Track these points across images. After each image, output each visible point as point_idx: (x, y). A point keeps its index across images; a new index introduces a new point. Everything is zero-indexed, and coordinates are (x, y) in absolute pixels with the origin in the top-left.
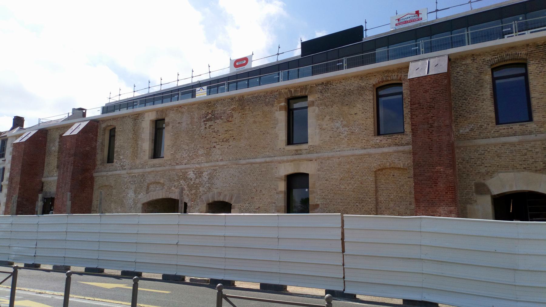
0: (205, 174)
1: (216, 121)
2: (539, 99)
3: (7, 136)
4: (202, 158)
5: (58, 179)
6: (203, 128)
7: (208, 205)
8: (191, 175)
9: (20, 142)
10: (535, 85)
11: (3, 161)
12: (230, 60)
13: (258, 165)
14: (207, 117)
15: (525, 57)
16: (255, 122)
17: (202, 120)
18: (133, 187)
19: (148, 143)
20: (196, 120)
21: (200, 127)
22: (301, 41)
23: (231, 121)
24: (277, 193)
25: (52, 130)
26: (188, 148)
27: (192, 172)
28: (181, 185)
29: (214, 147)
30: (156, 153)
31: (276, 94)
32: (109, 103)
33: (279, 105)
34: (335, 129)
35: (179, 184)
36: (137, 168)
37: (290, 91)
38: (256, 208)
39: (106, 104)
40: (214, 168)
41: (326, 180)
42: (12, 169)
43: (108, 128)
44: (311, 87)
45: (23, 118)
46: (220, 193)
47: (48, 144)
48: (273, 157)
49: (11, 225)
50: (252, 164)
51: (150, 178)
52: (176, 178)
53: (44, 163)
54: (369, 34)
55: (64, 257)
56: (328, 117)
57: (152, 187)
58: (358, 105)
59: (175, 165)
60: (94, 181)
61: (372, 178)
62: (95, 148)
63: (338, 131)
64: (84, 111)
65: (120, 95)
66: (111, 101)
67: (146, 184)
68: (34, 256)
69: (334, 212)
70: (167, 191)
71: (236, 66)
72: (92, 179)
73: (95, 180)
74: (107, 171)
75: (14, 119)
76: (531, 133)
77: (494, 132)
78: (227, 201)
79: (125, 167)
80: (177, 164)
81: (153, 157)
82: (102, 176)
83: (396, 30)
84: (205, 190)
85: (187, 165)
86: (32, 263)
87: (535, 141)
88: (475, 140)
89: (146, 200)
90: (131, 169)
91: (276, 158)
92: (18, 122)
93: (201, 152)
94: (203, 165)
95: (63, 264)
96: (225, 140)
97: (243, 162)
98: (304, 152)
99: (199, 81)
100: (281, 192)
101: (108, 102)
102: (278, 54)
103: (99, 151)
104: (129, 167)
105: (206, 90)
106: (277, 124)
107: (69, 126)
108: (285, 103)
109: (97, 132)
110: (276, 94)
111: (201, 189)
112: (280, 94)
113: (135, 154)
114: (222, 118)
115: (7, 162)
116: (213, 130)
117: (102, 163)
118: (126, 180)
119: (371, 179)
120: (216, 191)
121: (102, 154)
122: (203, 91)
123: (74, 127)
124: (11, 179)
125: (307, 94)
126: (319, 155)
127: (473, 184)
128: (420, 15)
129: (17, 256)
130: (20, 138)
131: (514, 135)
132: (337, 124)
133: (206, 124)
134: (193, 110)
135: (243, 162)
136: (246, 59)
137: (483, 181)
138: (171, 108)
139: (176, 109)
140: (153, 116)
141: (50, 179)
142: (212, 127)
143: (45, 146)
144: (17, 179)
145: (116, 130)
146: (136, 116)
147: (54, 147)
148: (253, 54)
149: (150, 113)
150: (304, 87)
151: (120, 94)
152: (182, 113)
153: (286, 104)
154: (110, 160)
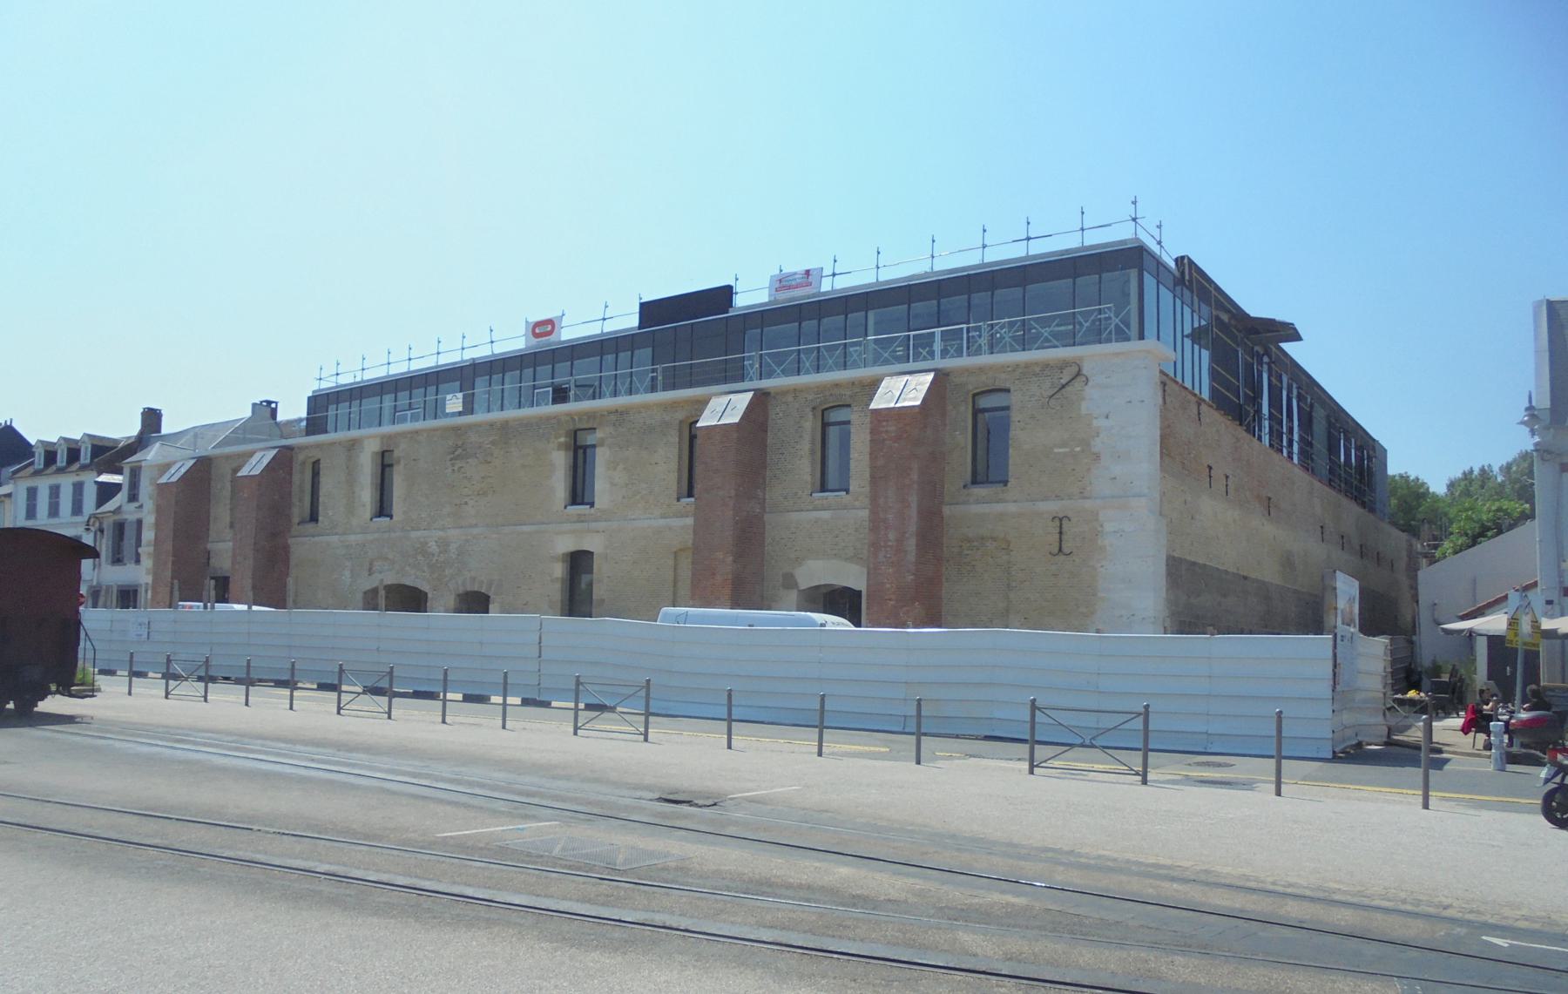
6: (450, 470)
9: (170, 481)
14: (456, 453)
19: (369, 490)
22: (641, 299)
27: (434, 543)
29: (466, 503)
30: (383, 509)
31: (553, 421)
33: (556, 442)
39: (314, 392)
42: (157, 525)
45: (160, 410)
46: (473, 579)
54: (741, 301)
56: (621, 467)
61: (671, 562)
64: (273, 405)
66: (325, 385)
71: (536, 335)
73: (292, 550)
80: (413, 529)
83: (775, 301)
99: (473, 359)
100: (557, 578)
101: (316, 388)
103: (295, 500)
105: (461, 400)
108: (566, 437)
109: (291, 469)
110: (553, 421)
111: (447, 572)
115: (145, 509)
121: (300, 508)
123: (254, 460)
124: (157, 542)
136: (550, 322)
138: (403, 435)
140: (371, 448)
141: (221, 546)
142: (463, 470)
147: (222, 489)
150: (591, 415)
153: (568, 439)
154: (314, 518)
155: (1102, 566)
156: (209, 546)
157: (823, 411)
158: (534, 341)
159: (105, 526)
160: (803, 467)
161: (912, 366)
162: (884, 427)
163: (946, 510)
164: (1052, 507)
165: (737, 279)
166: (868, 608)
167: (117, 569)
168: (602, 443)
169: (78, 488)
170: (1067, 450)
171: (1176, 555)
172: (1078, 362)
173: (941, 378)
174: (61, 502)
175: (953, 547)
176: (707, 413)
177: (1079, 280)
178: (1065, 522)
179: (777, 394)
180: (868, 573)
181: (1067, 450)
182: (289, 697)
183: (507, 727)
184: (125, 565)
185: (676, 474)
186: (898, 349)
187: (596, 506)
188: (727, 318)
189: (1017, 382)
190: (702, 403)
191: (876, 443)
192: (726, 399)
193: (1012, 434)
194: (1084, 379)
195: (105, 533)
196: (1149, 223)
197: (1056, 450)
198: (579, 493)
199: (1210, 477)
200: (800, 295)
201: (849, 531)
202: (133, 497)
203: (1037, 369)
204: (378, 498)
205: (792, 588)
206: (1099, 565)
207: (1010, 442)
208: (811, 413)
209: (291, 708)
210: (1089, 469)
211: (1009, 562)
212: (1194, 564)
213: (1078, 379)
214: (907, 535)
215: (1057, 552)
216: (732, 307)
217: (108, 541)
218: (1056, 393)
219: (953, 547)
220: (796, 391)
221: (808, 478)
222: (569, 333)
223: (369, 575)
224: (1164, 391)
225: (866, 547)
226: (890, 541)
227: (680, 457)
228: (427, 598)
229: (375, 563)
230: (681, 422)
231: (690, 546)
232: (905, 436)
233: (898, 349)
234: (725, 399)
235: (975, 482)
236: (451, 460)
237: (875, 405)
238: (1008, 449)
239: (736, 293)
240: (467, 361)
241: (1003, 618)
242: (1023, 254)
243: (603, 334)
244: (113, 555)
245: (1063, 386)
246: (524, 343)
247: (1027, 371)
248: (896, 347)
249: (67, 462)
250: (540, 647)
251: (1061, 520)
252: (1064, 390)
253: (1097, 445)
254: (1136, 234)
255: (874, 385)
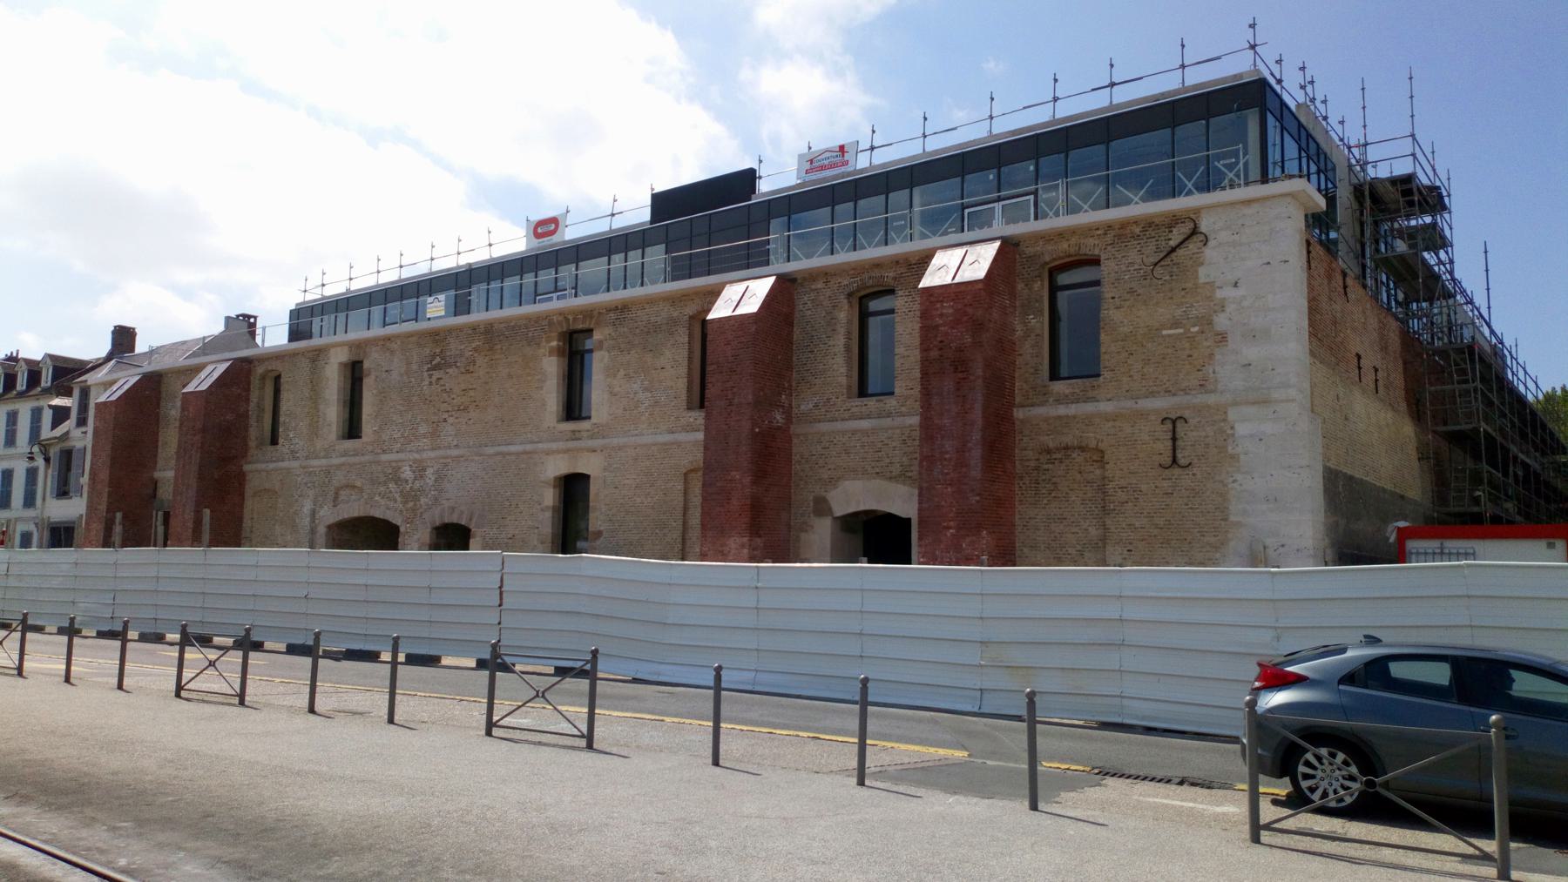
0: (429, 471)
1: (448, 370)
2: (904, 357)
3: (89, 383)
4: (425, 440)
5: (176, 478)
7: (434, 531)
8: (407, 473)
10: (901, 332)
11: (82, 433)
12: (525, 222)
13: (513, 458)
14: (434, 363)
15: (892, 282)
16: (510, 376)
17: (426, 368)
18: (311, 493)
20: (415, 367)
21: (422, 380)
22: (653, 190)
23: (472, 372)
24: (542, 510)
25: (170, 375)
26: (401, 421)
27: (408, 468)
28: (391, 492)
29: (445, 420)
30: (352, 429)
32: (304, 303)
34: (631, 396)
35: (388, 491)
36: (317, 457)
37: (567, 320)
38: (509, 536)
39: (297, 305)
40: (445, 461)
41: (616, 488)
43: (270, 374)
44: (600, 313)
45: (134, 329)
46: (453, 509)
47: (163, 404)
48: (536, 443)
49: (74, 565)
50: (503, 454)
51: (339, 478)
52: (382, 479)
53: (157, 441)
54: (766, 186)
55: (156, 619)
57: (343, 494)
58: (667, 352)
59: (379, 454)
60: (244, 480)
61: (680, 487)
62: (246, 415)
63: (636, 399)
64: (252, 320)
65: (323, 285)
66: (310, 297)
67: (332, 488)
68: (112, 618)
69: (1186, 563)
70: (366, 503)
71: (537, 235)
72: (241, 478)
73: (247, 478)
74: (267, 462)
75: (113, 333)
76: (889, 415)
77: (845, 410)
78: (463, 523)
79: (298, 455)
80: (384, 452)
81: (347, 435)
82: (259, 472)
84: (430, 503)
85: (400, 454)
86: (107, 630)
87: (892, 428)
88: (817, 425)
89: (332, 520)
90: (307, 458)
91: (540, 446)
92: (123, 338)
93: (423, 429)
94: (425, 455)
95: (153, 631)
96: (462, 408)
97: (490, 450)
98: (585, 434)
99: (470, 265)
100: (547, 507)
101: (300, 300)
102: (613, 215)
103: (253, 422)
104: (305, 455)
105: (443, 303)
106: (544, 381)
107: (197, 369)
108: (559, 340)
109: (249, 384)
111: (423, 500)
112: (551, 324)
113: (314, 430)
114: (458, 364)
116: (443, 388)
117: (260, 445)
118: (299, 479)
119: (679, 487)
120: (446, 504)
121: (258, 429)
122: (440, 304)
123: (203, 375)
125: (592, 326)
126: (606, 441)
127: (811, 498)
128: (846, 154)
129: (85, 618)
130: (108, 393)
131: (869, 417)
132: (636, 385)
133: (430, 376)
134: (410, 346)
135: (490, 450)
137: (824, 494)
139: (382, 343)
140: (340, 357)
142: (442, 382)
143: (159, 408)
144: (104, 475)
145: (282, 380)
146: (315, 353)
147: (173, 411)
148: (568, 212)
149: (339, 349)
150: (588, 313)
151: (325, 283)
152: (392, 352)
153: (561, 344)
154: (274, 441)
155: (1234, 481)
156: (157, 475)
157: (861, 299)
158: (536, 243)
159: (51, 455)
160: (837, 367)
161: (968, 235)
162: (937, 309)
163: (1019, 414)
164: (1161, 403)
165: (760, 161)
166: (920, 539)
167: (64, 502)
168: (600, 345)
169: (36, 415)
170: (1181, 331)
171: (1332, 466)
172: (1193, 217)
173: (1009, 249)
174: (5, 425)
175: (1028, 460)
176: (720, 302)
177: (1180, 131)
178: (1179, 424)
179: (805, 279)
180: (920, 495)
181: (1181, 331)
182: (176, 662)
183: (397, 718)
184: (71, 498)
185: (686, 380)
186: (950, 230)
187: (594, 420)
188: (749, 205)
189: (1109, 248)
190: (714, 294)
191: (928, 330)
192: (742, 286)
193: (1104, 313)
194: (1202, 238)
195: (52, 461)
196: (1268, 54)
197: (1165, 332)
198: (573, 408)
199: (1360, 368)
200: (830, 176)
201: (894, 444)
202: (82, 422)
203: (1137, 230)
204: (347, 416)
205: (827, 515)
206: (1231, 480)
207: (1102, 324)
208: (846, 301)
209: (120, 687)
210: (1211, 355)
211: (1104, 478)
212: (1351, 478)
213: (1195, 238)
214: (970, 445)
215: (1170, 463)
216: (755, 193)
217: (53, 472)
218: (1162, 259)
219: (1028, 460)
220: (825, 274)
221: (843, 380)
222: (572, 233)
223: (334, 506)
224: (1309, 252)
225: (916, 463)
226: (947, 453)
227: (690, 359)
228: (399, 531)
229: (342, 492)
230: (692, 318)
231: (702, 465)
232: (965, 319)
233: (950, 230)
234: (740, 287)
235: (1054, 375)
236: (429, 370)
237: (926, 282)
238: (1099, 333)
239: (760, 177)
240: (462, 267)
241: (1096, 551)
242: (1106, 103)
243: (611, 231)
244: (58, 489)
245: (1173, 250)
246: (525, 244)
247: (1121, 233)
248: (947, 229)
249: (27, 386)
250: (501, 593)
251: (1174, 422)
252: (1174, 254)
253: (1221, 322)
254: (1255, 66)
255: (924, 260)
